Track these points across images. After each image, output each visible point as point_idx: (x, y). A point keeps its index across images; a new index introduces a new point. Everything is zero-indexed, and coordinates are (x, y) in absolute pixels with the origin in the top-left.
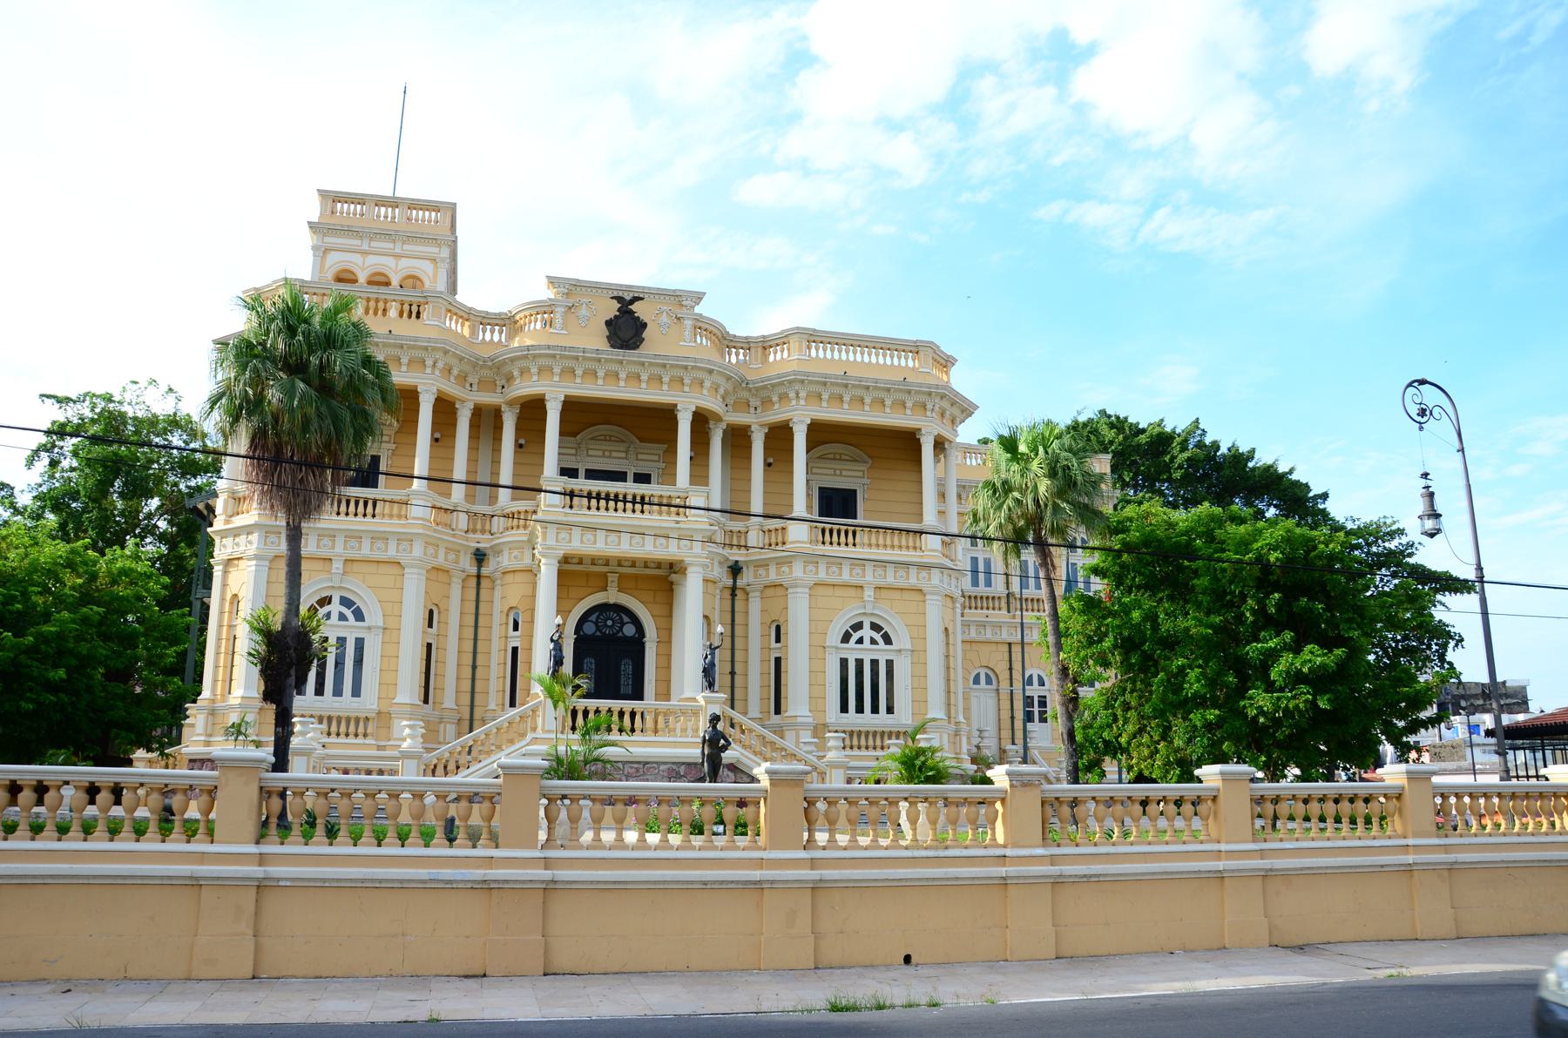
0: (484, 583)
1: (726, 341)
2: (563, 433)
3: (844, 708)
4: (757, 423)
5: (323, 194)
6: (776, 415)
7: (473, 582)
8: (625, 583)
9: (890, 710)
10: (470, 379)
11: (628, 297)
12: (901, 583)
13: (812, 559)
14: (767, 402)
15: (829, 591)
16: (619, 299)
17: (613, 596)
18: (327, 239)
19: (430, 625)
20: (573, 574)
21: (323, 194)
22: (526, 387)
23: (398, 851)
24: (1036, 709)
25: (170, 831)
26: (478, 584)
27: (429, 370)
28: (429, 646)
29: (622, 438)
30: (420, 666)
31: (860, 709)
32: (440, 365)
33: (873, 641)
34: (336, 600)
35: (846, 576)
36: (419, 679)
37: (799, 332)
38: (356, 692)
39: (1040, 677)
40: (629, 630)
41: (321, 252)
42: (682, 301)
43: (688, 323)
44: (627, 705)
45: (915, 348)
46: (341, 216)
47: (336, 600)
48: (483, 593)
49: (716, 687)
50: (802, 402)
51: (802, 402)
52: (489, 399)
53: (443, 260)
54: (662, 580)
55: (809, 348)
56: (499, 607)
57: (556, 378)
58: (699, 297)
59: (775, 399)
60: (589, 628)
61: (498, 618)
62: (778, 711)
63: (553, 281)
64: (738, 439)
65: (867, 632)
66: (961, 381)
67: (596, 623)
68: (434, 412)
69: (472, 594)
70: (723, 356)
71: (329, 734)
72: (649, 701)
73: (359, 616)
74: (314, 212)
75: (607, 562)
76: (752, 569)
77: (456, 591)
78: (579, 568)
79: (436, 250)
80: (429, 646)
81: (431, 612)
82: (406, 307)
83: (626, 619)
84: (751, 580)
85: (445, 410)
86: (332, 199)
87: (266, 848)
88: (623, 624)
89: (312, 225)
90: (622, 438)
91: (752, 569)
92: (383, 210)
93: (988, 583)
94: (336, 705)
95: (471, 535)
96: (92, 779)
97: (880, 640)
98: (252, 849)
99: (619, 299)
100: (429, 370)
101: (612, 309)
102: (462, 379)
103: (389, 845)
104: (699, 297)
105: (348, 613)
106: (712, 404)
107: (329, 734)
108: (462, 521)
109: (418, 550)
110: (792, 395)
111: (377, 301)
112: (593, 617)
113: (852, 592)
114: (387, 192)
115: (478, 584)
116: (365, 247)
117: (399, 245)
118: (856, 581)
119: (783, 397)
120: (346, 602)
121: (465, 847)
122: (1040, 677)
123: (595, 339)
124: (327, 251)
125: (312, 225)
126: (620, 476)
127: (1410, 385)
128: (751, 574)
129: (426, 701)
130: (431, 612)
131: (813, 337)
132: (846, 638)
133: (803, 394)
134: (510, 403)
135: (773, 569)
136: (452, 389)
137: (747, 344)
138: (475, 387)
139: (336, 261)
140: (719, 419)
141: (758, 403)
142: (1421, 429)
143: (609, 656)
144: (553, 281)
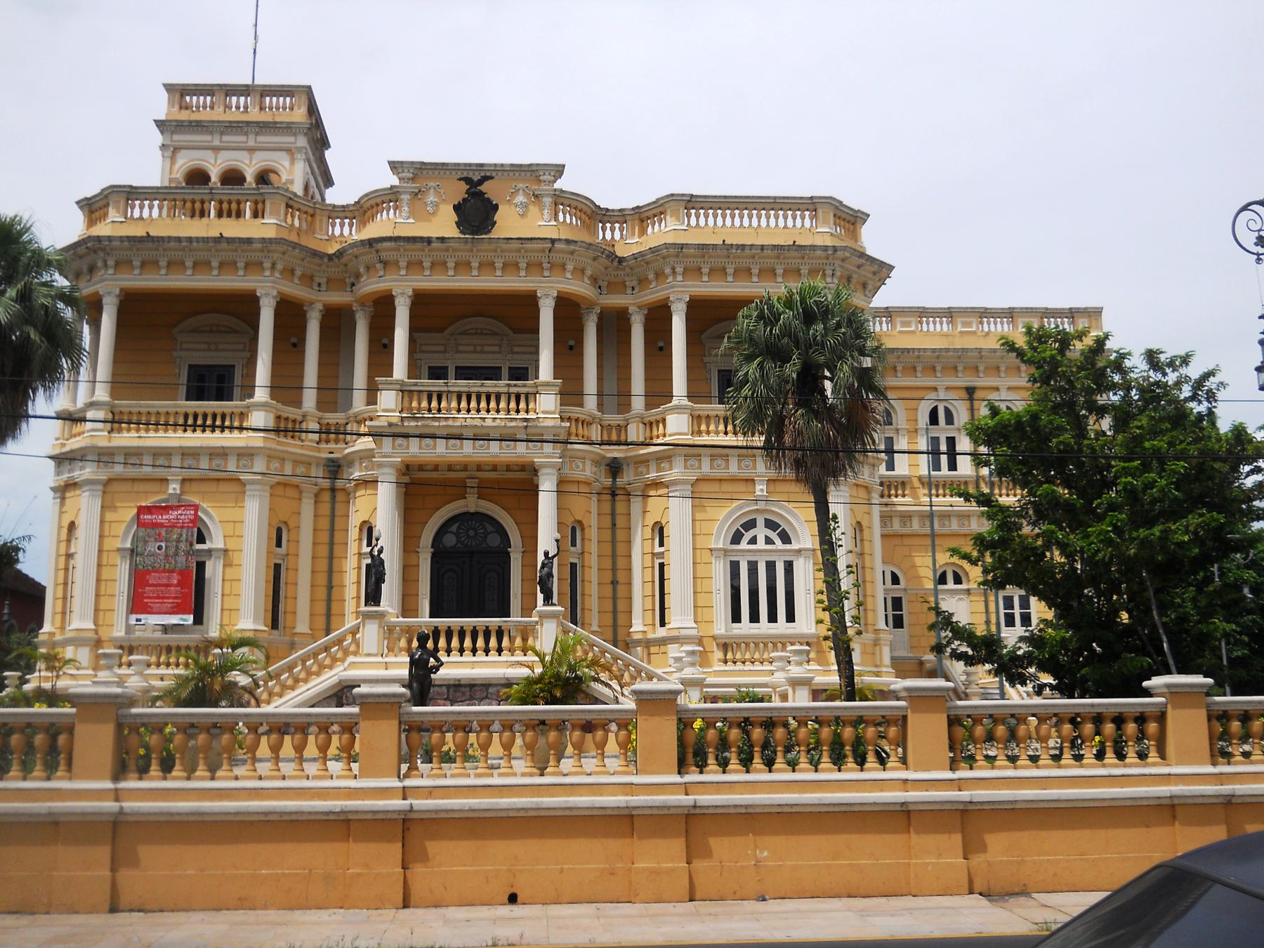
0: (340, 497)
1: (594, 214)
2: (413, 329)
3: (736, 618)
4: (633, 302)
5: (169, 88)
6: (652, 295)
7: (326, 496)
8: (487, 489)
9: (791, 618)
10: (317, 280)
11: (476, 178)
12: (719, 473)
13: (691, 451)
14: (643, 282)
15: (715, 487)
16: (467, 180)
17: (472, 503)
18: (176, 137)
19: (279, 544)
20: (417, 488)
21: (169, 88)
22: (372, 285)
23: (812, 776)
24: (1017, 611)
25: (706, 765)
26: (333, 498)
27: (267, 273)
28: (277, 567)
29: (474, 334)
30: (266, 589)
31: (754, 618)
32: (679, 270)
33: (769, 541)
34: (760, 522)
35: (734, 468)
36: (265, 603)
37: (672, 197)
38: (791, 618)
39: (893, 574)
40: (494, 541)
41: (170, 151)
42: (536, 177)
43: (548, 200)
44: (494, 622)
45: (811, 205)
46: (192, 112)
47: (760, 522)
48: (338, 506)
49: (555, 600)
50: (680, 278)
51: (680, 278)
52: (337, 298)
53: (299, 149)
54: (519, 487)
55: (689, 216)
56: (355, 520)
57: (403, 272)
58: (559, 170)
59: (651, 276)
60: (450, 540)
61: (353, 533)
62: (663, 624)
63: (395, 166)
64: (614, 327)
65: (761, 532)
66: (872, 241)
67: (457, 534)
68: (276, 315)
69: (325, 509)
70: (596, 233)
71: (726, 662)
72: (515, 618)
73: (785, 538)
74: (161, 107)
75: (465, 468)
76: (632, 466)
77: (307, 507)
78: (434, 475)
79: (291, 139)
80: (277, 567)
81: (279, 531)
82: (225, 206)
83: (490, 528)
84: (632, 478)
85: (290, 317)
86: (180, 92)
87: (688, 778)
88: (487, 534)
89: (160, 124)
90: (474, 334)
91: (632, 466)
92: (234, 99)
93: (953, 466)
94: (736, 632)
95: (323, 446)
96: (746, 715)
97: (778, 541)
98: (676, 778)
99: (467, 180)
100: (267, 273)
101: (459, 191)
102: (308, 279)
103: (779, 771)
104: (559, 170)
105: (774, 536)
106: (579, 288)
107: (726, 662)
108: (595, 433)
109: (259, 465)
110: (668, 271)
111: (230, 202)
112: (454, 528)
113: (741, 487)
114: (244, 79)
115: (333, 498)
116: (217, 143)
117: (252, 137)
118: (746, 473)
119: (659, 275)
120: (771, 525)
121: (716, 772)
122: (893, 574)
123: (444, 224)
124: (176, 150)
125: (160, 124)
126: (493, 373)
127: (1245, 208)
128: (632, 472)
129: (275, 625)
130: (279, 531)
131: (692, 203)
132: (737, 539)
133: (679, 270)
134: (362, 302)
135: (653, 466)
136: (295, 290)
137: (621, 217)
138: (323, 287)
139: (185, 161)
140: (591, 305)
141: (634, 283)
142: (1259, 260)
143: (469, 569)
144: (395, 166)
